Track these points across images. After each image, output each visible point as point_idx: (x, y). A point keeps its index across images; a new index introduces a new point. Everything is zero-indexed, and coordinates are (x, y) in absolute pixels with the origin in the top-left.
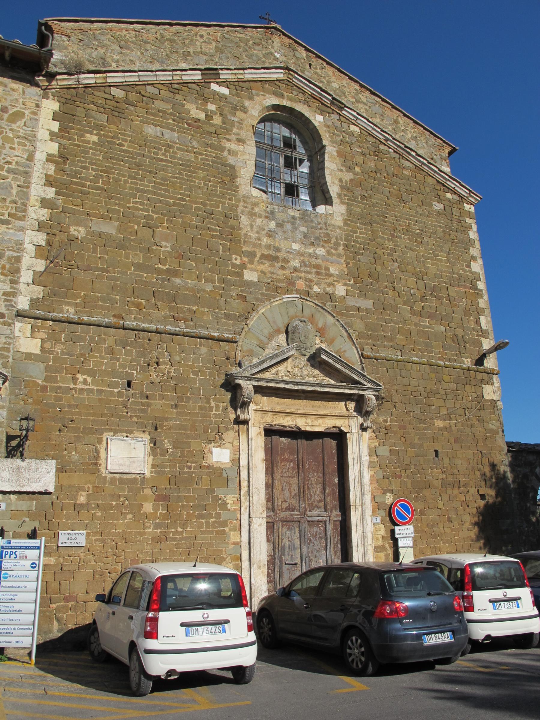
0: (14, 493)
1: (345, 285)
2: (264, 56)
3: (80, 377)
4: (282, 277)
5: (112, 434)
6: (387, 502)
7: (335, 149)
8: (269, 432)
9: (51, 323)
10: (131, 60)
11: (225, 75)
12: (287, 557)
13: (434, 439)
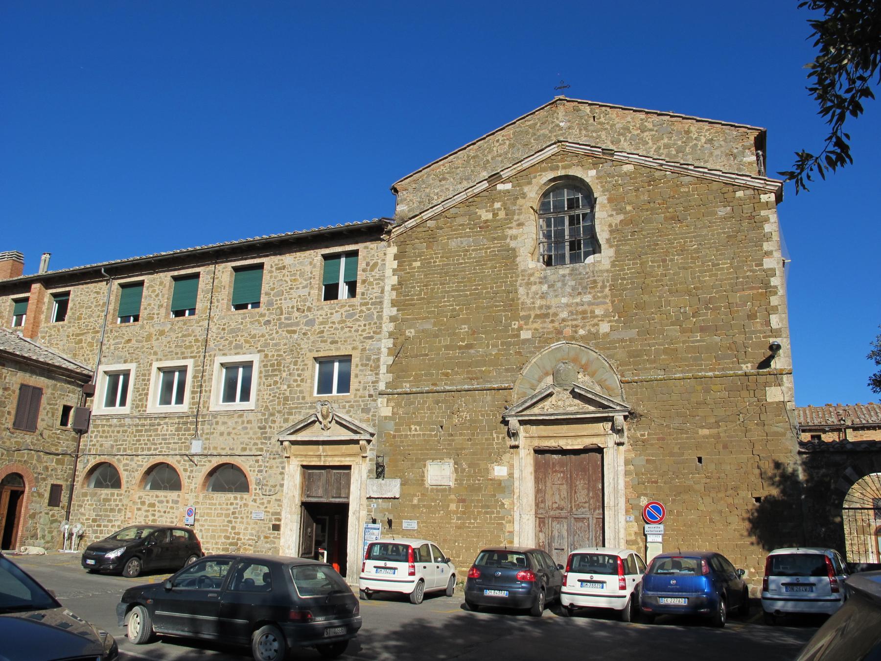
0: (381, 498)
1: (610, 321)
2: (550, 132)
3: (413, 427)
4: (552, 329)
5: (431, 461)
6: (641, 504)
7: (606, 197)
8: (538, 451)
9: (396, 396)
10: (446, 189)
11: (505, 174)
12: (556, 544)
13: (698, 446)
